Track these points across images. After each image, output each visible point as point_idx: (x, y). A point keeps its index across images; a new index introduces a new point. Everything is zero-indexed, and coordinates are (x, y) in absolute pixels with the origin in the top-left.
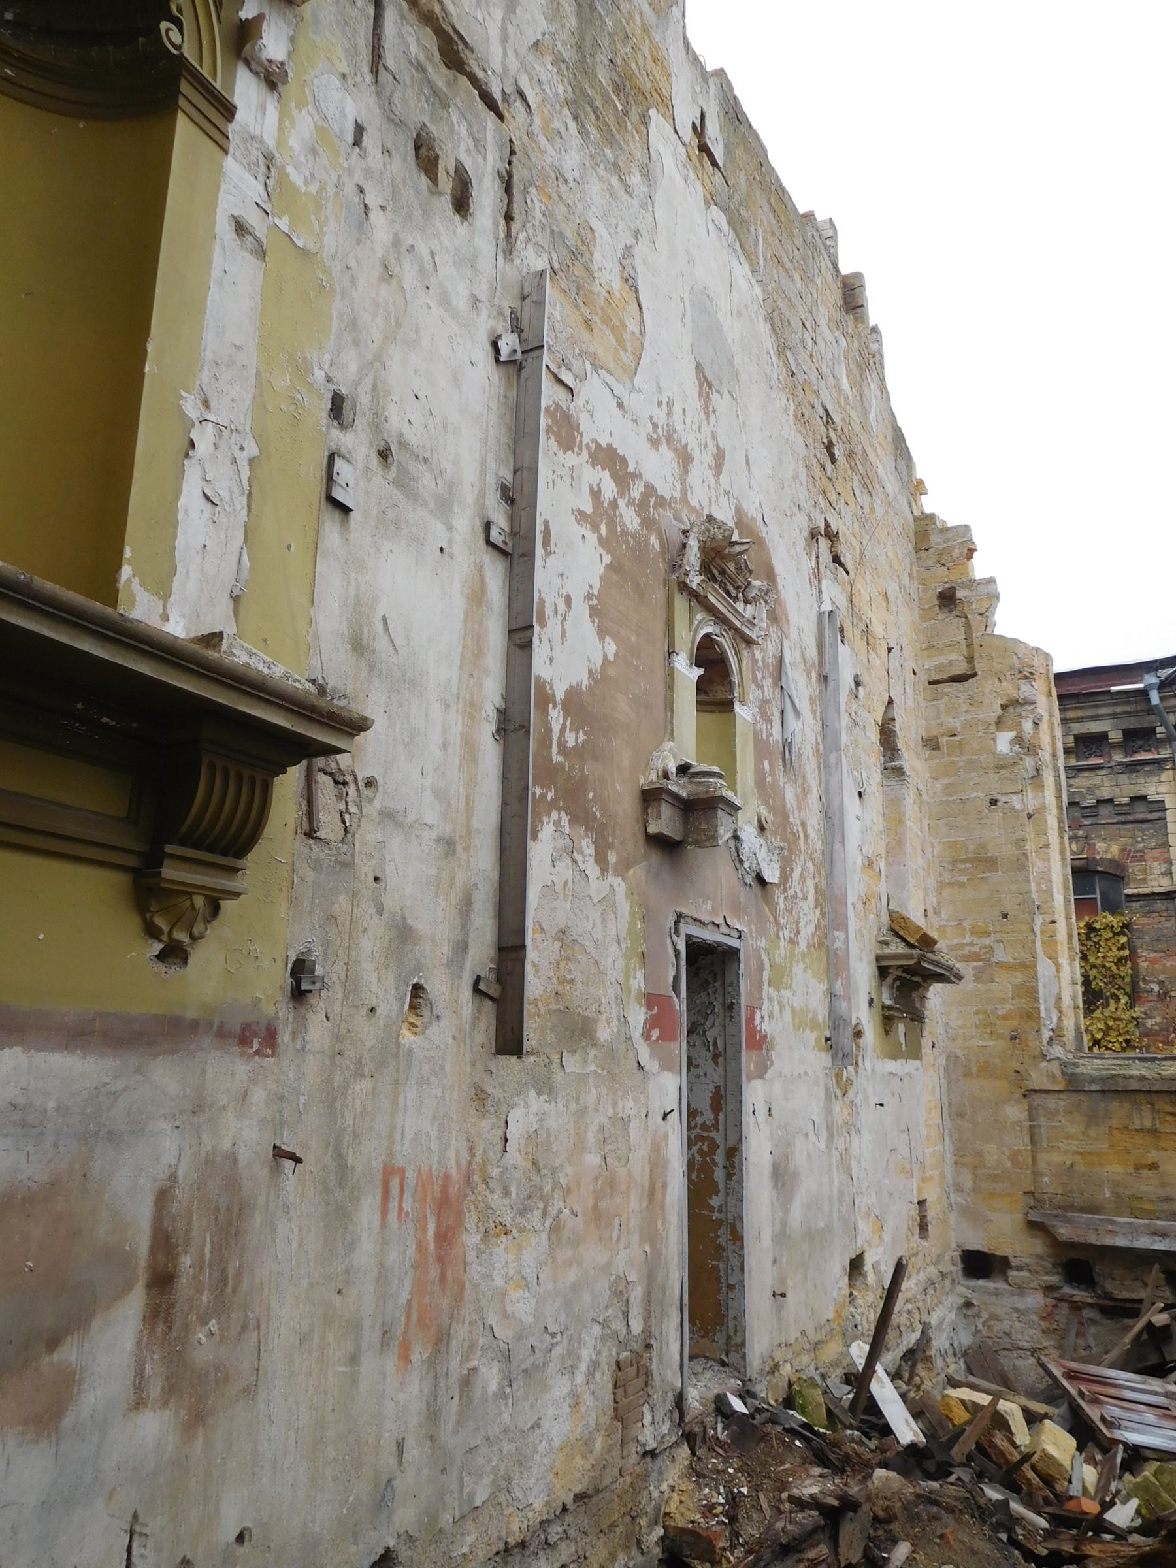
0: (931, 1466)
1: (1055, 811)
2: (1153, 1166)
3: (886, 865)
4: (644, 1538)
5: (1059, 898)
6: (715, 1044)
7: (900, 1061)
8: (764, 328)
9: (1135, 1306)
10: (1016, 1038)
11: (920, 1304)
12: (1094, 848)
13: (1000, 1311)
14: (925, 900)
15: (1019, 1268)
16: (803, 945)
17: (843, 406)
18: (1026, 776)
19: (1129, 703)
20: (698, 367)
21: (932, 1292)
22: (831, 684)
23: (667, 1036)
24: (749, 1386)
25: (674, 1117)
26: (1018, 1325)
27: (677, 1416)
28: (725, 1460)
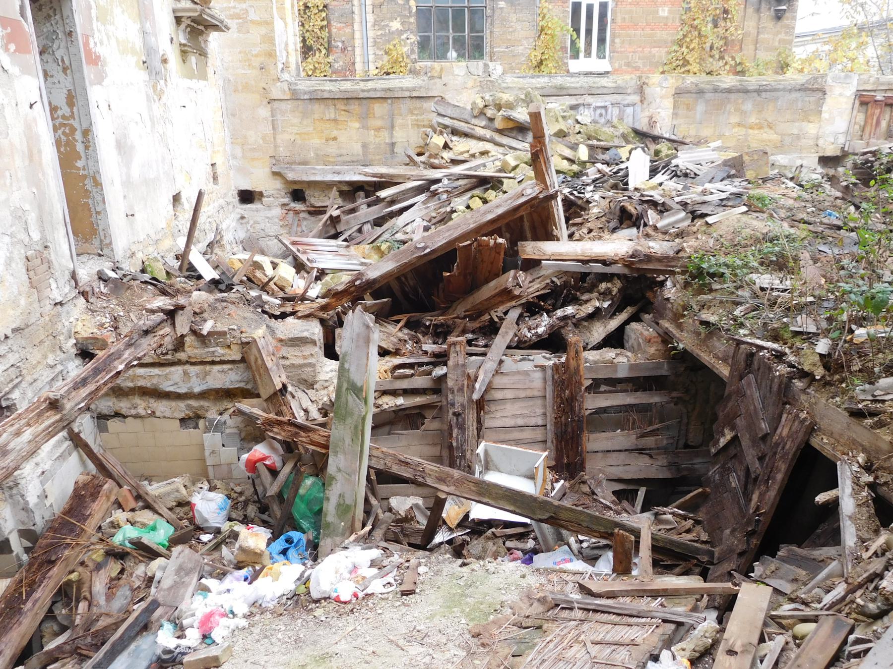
0: (223, 287)
2: (335, 139)
4: (64, 345)
6: (63, 61)
11: (216, 219)
13: (259, 219)
15: (268, 197)
23: (22, 49)
24: (118, 265)
25: (38, 107)
26: (268, 225)
27: (73, 283)
28: (108, 301)
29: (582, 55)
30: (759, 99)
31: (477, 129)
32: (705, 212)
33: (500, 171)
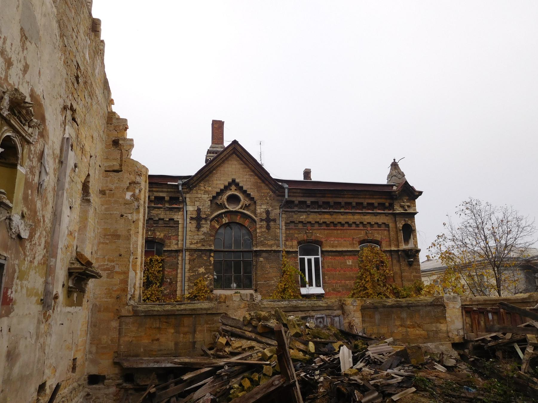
1: (142, 221)
2: (158, 340)
3: (78, 234)
5: (139, 250)
7: (73, 307)
8: (55, 25)
9: (146, 387)
10: (118, 298)
11: (68, 398)
12: (156, 234)
14: (92, 248)
15: (109, 379)
16: (36, 263)
17: (85, 64)
18: (134, 208)
19: (172, 188)
20: (22, 29)
21: (74, 392)
22: (64, 165)
26: (105, 399)
29: (307, 285)
30: (409, 311)
31: (247, 333)
32: (390, 392)
33: (260, 360)
